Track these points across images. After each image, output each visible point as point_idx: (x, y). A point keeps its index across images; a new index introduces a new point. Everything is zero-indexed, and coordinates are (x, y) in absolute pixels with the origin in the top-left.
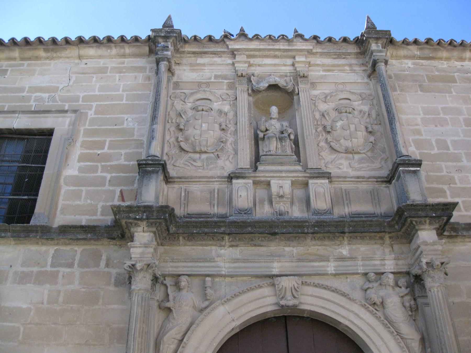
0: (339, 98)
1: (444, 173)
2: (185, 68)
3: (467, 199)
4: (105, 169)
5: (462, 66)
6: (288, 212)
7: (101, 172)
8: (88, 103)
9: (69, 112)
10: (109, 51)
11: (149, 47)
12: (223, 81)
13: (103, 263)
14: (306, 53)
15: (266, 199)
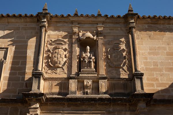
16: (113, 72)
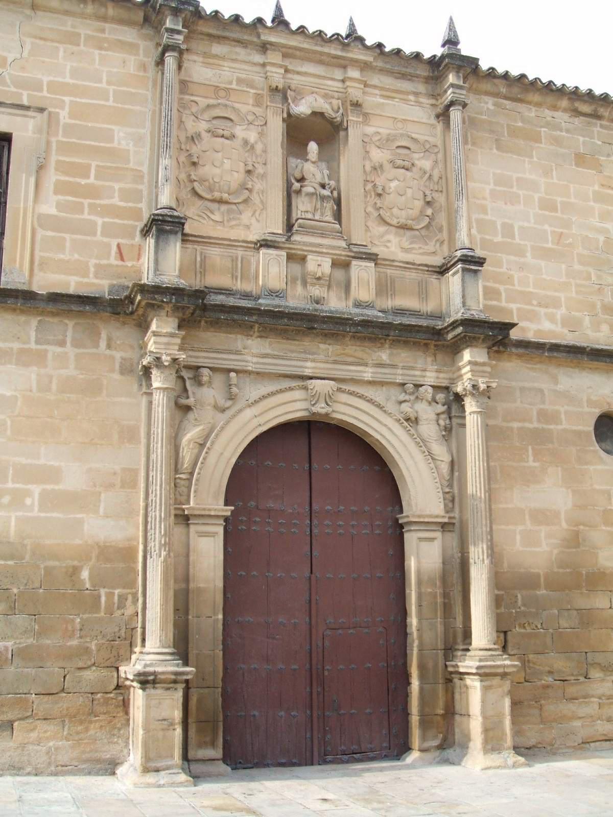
0: (397, 145)
1: (504, 270)
2: (195, 57)
3: (522, 306)
4: (93, 208)
6: (324, 298)
7: (89, 214)
8: (58, 97)
9: (32, 109)
10: (82, 6)
11: (145, 12)
12: (248, 90)
14: (362, 65)
15: (299, 277)
16: (389, 241)
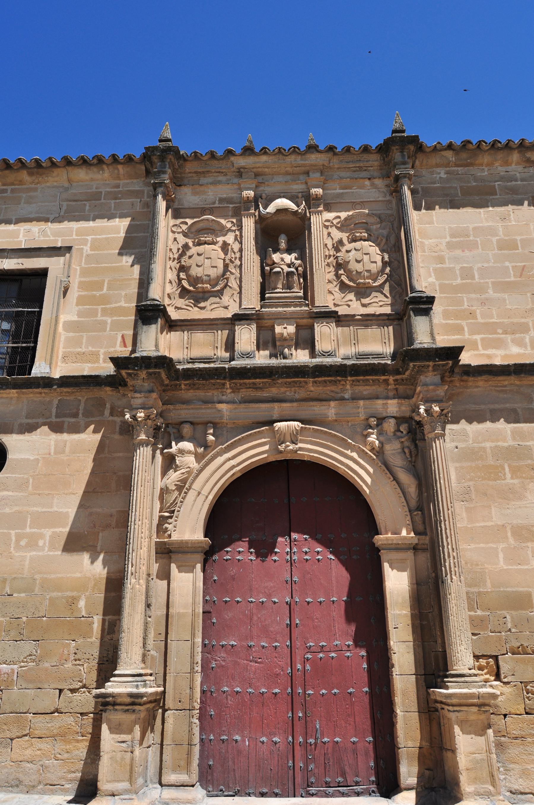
4: (105, 312)
5: (506, 172)
13: (107, 412)
15: (270, 341)
